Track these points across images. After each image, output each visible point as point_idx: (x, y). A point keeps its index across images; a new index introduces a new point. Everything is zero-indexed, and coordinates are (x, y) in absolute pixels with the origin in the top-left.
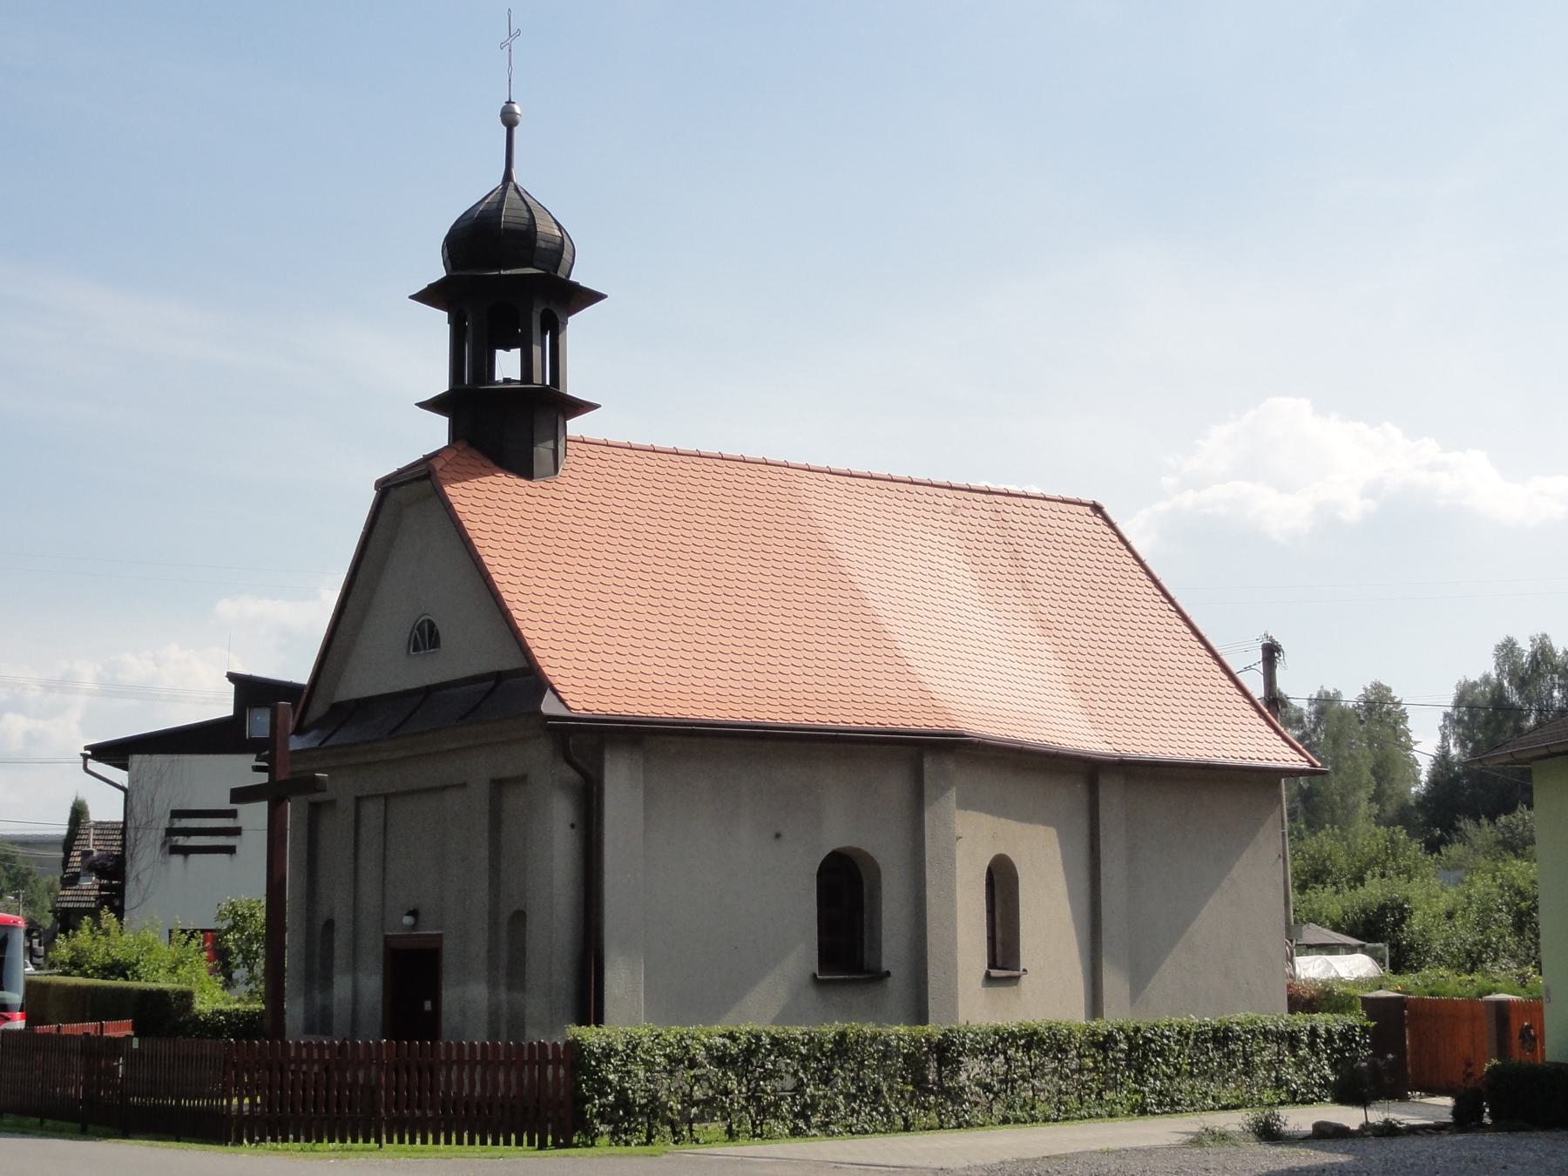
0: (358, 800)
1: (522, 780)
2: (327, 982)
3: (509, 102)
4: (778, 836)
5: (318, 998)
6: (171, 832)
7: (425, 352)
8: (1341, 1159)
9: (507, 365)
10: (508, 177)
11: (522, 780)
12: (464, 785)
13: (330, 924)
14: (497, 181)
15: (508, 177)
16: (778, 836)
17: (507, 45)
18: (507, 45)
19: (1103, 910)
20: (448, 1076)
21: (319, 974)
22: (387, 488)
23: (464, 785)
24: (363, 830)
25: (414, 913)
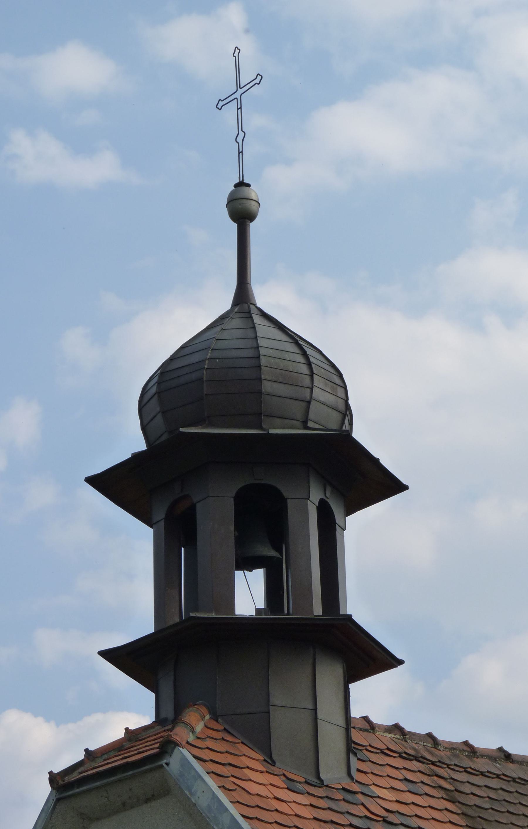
3: (241, 184)
10: (243, 295)
15: (243, 295)
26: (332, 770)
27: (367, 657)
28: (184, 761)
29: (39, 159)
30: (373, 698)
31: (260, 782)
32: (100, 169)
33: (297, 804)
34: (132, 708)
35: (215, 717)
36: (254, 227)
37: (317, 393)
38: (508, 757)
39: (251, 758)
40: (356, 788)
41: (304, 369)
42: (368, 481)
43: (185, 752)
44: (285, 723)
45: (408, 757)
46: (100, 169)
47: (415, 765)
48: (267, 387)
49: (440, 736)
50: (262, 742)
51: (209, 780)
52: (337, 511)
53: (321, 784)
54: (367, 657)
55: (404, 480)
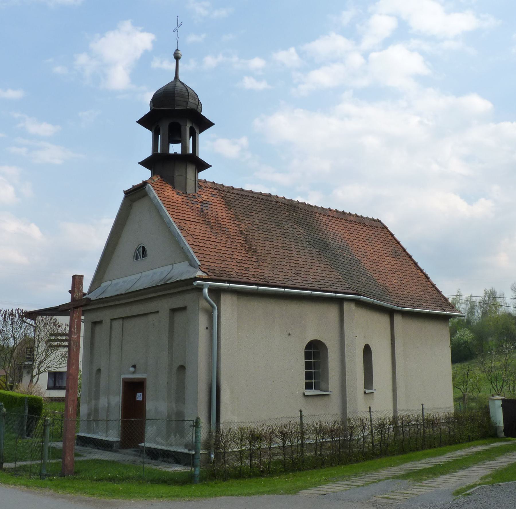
0: (112, 320)
1: (184, 309)
2: (97, 398)
3: (177, 50)
4: (289, 335)
5: (93, 402)
6: (49, 340)
7: (144, 142)
8: (80, 367)
9: (175, 149)
10: (176, 77)
11: (184, 309)
12: (158, 312)
13: (99, 370)
14: (172, 79)
15: (176, 77)
16: (289, 335)
17: (176, 30)
18: (176, 30)
19: (396, 366)
20: (64, 341)
21: (95, 393)
22: (127, 193)
23: (158, 312)
24: (113, 333)
25: (134, 366)
26: (190, 190)
27: (203, 166)
28: (149, 188)
29: (249, 83)
30: (203, 175)
31: (169, 191)
32: (262, 86)
33: (178, 198)
34: (146, 174)
35: (162, 177)
36: (180, 61)
37: (190, 100)
38: (242, 190)
39: (168, 187)
40: (196, 195)
41: (187, 94)
42: (205, 124)
43: (149, 185)
44: (178, 179)
45: (215, 189)
46: (262, 86)
47: (216, 191)
48: (177, 98)
49: (224, 185)
50: (172, 183)
51: (154, 191)
52: (197, 131)
53: (186, 193)
54: (203, 166)
55: (213, 122)
